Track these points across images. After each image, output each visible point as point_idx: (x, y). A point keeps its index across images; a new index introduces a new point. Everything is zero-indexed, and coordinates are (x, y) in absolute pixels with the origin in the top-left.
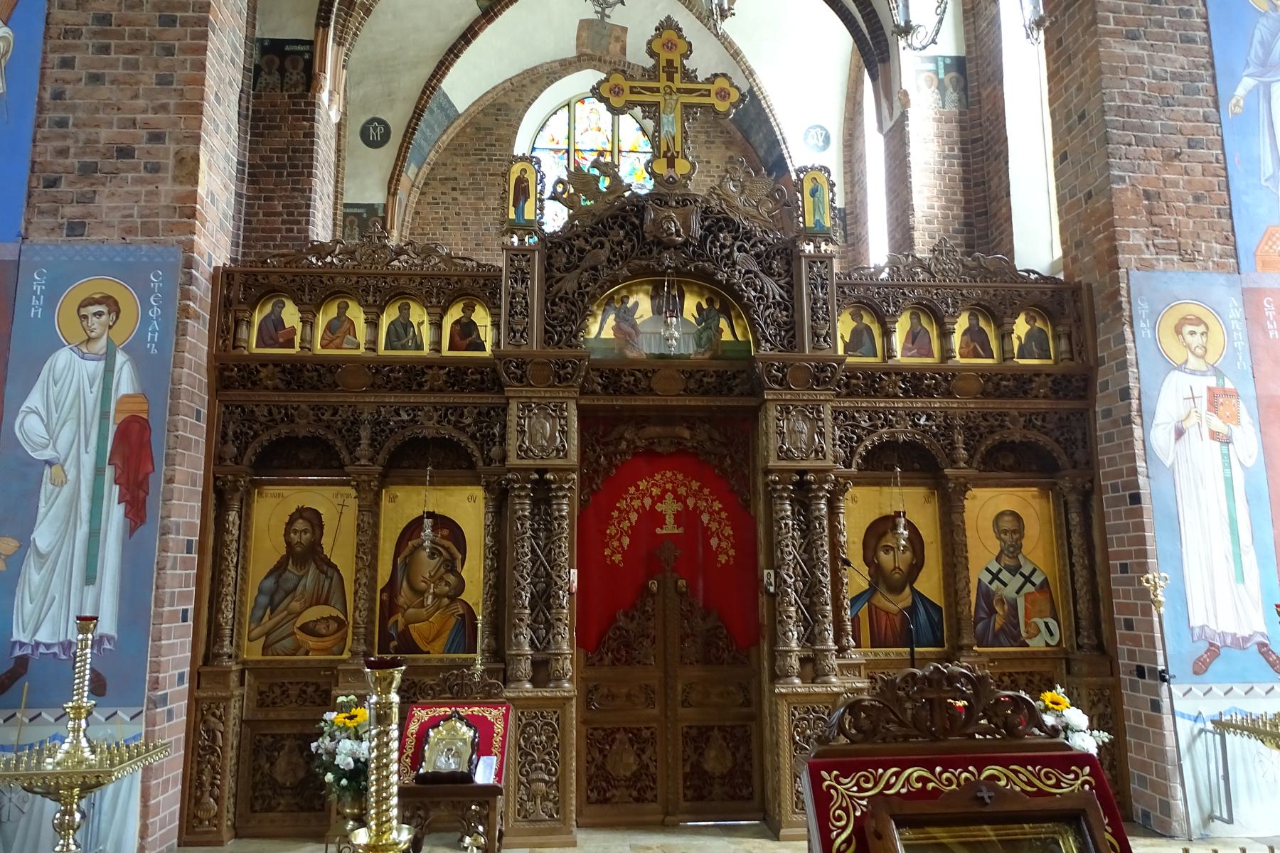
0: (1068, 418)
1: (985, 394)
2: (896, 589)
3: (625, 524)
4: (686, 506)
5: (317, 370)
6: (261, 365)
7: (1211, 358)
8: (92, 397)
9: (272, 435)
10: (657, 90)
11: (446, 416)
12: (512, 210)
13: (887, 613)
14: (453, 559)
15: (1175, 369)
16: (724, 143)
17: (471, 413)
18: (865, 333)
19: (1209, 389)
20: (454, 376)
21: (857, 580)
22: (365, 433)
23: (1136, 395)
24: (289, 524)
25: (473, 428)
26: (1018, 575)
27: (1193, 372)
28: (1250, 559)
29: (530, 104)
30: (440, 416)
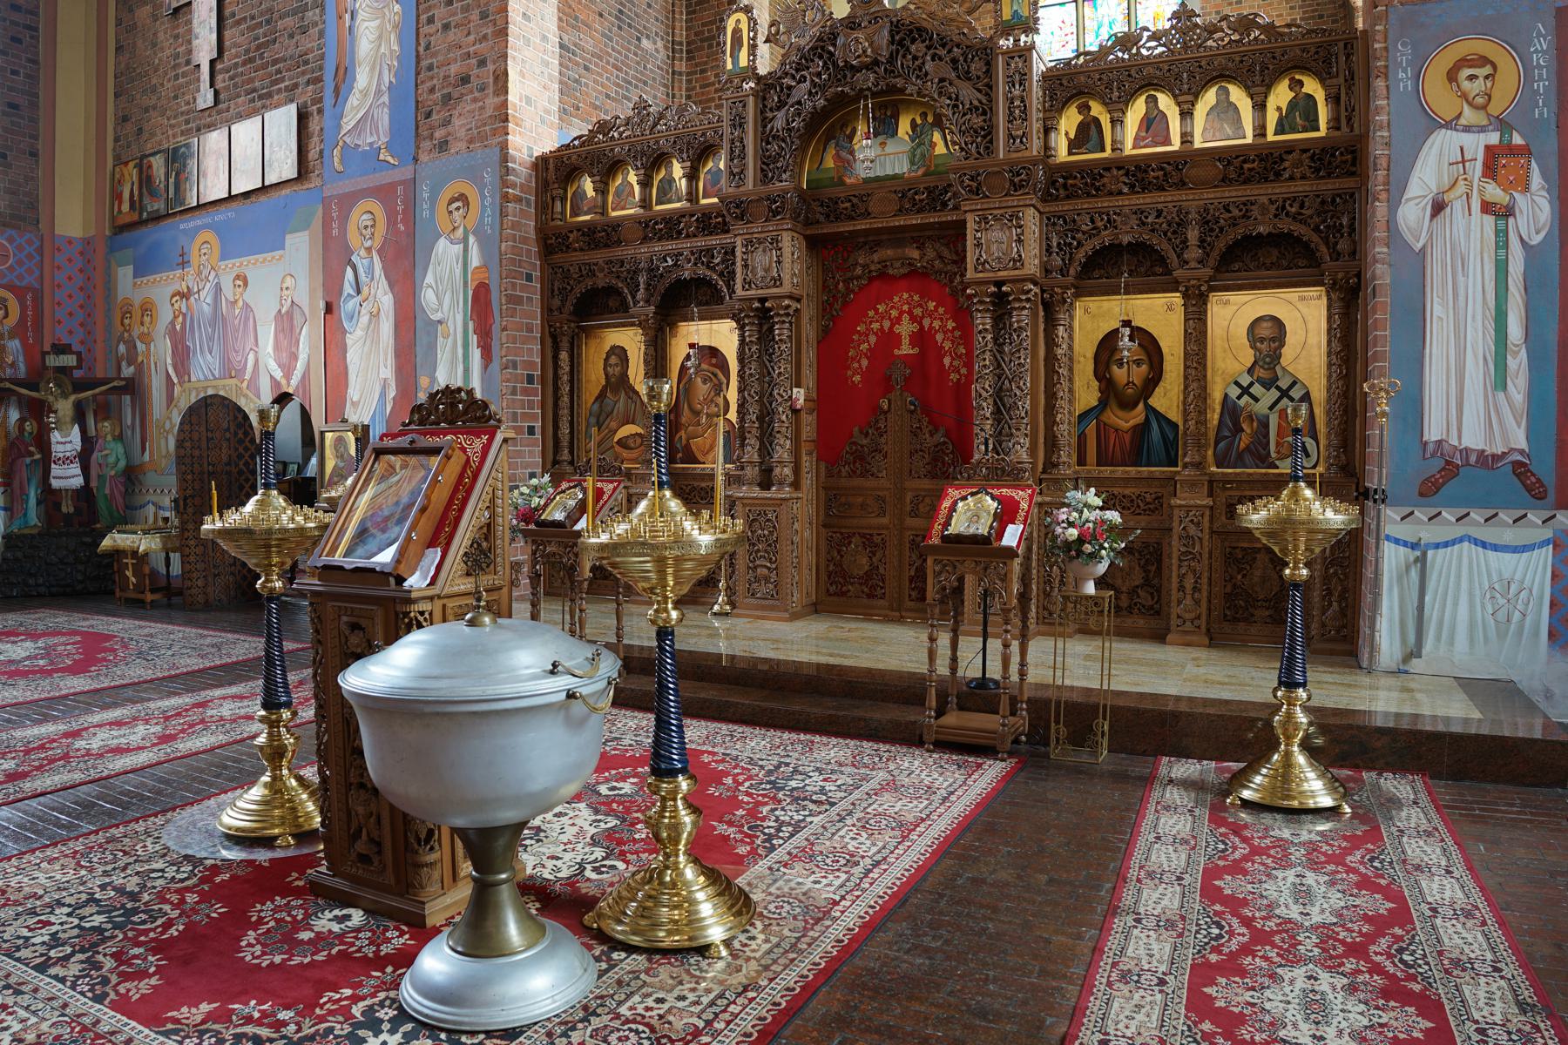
0: (1334, 200)
1: (1225, 180)
2: (1128, 405)
3: (864, 347)
4: (922, 327)
5: (1162, 169)
6: (1104, 169)
7: (1494, 109)
8: (458, 271)
9: (1096, 243)
11: (1284, 207)
12: (729, 60)
13: (1117, 430)
14: (721, 384)
15: (1442, 126)
17: (719, 253)
18: (1093, 127)
19: (1488, 148)
20: (1319, 159)
21: (1086, 393)
22: (1193, 235)
23: (1385, 165)
24: (606, 360)
25: (722, 267)
26: (1273, 390)
27: (1467, 129)
28: (1518, 362)
30: (1277, 209)
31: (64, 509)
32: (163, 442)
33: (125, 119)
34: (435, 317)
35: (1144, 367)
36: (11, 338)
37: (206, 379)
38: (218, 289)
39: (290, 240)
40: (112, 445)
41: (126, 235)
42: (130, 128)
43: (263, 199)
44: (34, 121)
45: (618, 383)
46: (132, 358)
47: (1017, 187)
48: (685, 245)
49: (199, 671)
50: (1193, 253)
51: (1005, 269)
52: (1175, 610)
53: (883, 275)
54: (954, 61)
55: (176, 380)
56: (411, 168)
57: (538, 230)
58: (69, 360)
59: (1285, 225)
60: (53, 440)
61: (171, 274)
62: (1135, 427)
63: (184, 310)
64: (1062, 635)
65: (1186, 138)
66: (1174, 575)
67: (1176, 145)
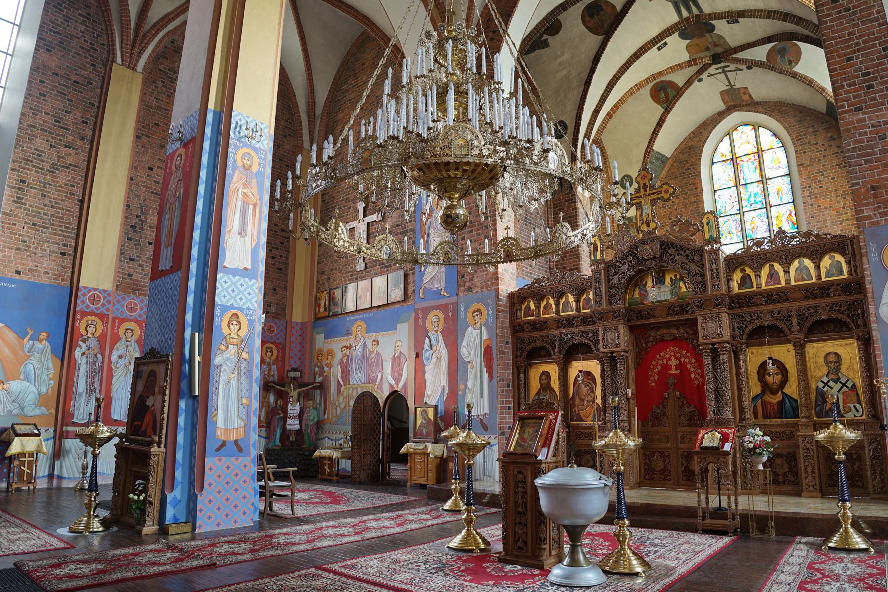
1: (806, 298)
2: (774, 392)
3: (656, 370)
4: (680, 362)
8: (477, 341)
9: (754, 326)
10: (641, 197)
11: (833, 308)
16: (825, 129)
21: (756, 389)
22: (795, 321)
24: (540, 377)
29: (705, 141)
31: (291, 439)
32: (334, 410)
33: (322, 273)
34: (467, 360)
35: (780, 376)
36: (273, 364)
37: (358, 384)
38: (365, 345)
39: (399, 326)
40: (312, 411)
41: (321, 321)
42: (324, 277)
43: (387, 308)
44: (286, 275)
45: (546, 387)
46: (321, 373)
47: (718, 305)
48: (575, 330)
49: (344, 511)
50: (795, 328)
51: (715, 338)
52: (804, 482)
53: (662, 340)
54: (687, 255)
55: (342, 384)
56: (455, 298)
57: (511, 323)
58: (298, 374)
59: (834, 315)
60: (289, 408)
61: (342, 339)
62: (778, 402)
63: (348, 354)
64: (751, 494)
65: (788, 281)
66: (802, 465)
67: (783, 284)
